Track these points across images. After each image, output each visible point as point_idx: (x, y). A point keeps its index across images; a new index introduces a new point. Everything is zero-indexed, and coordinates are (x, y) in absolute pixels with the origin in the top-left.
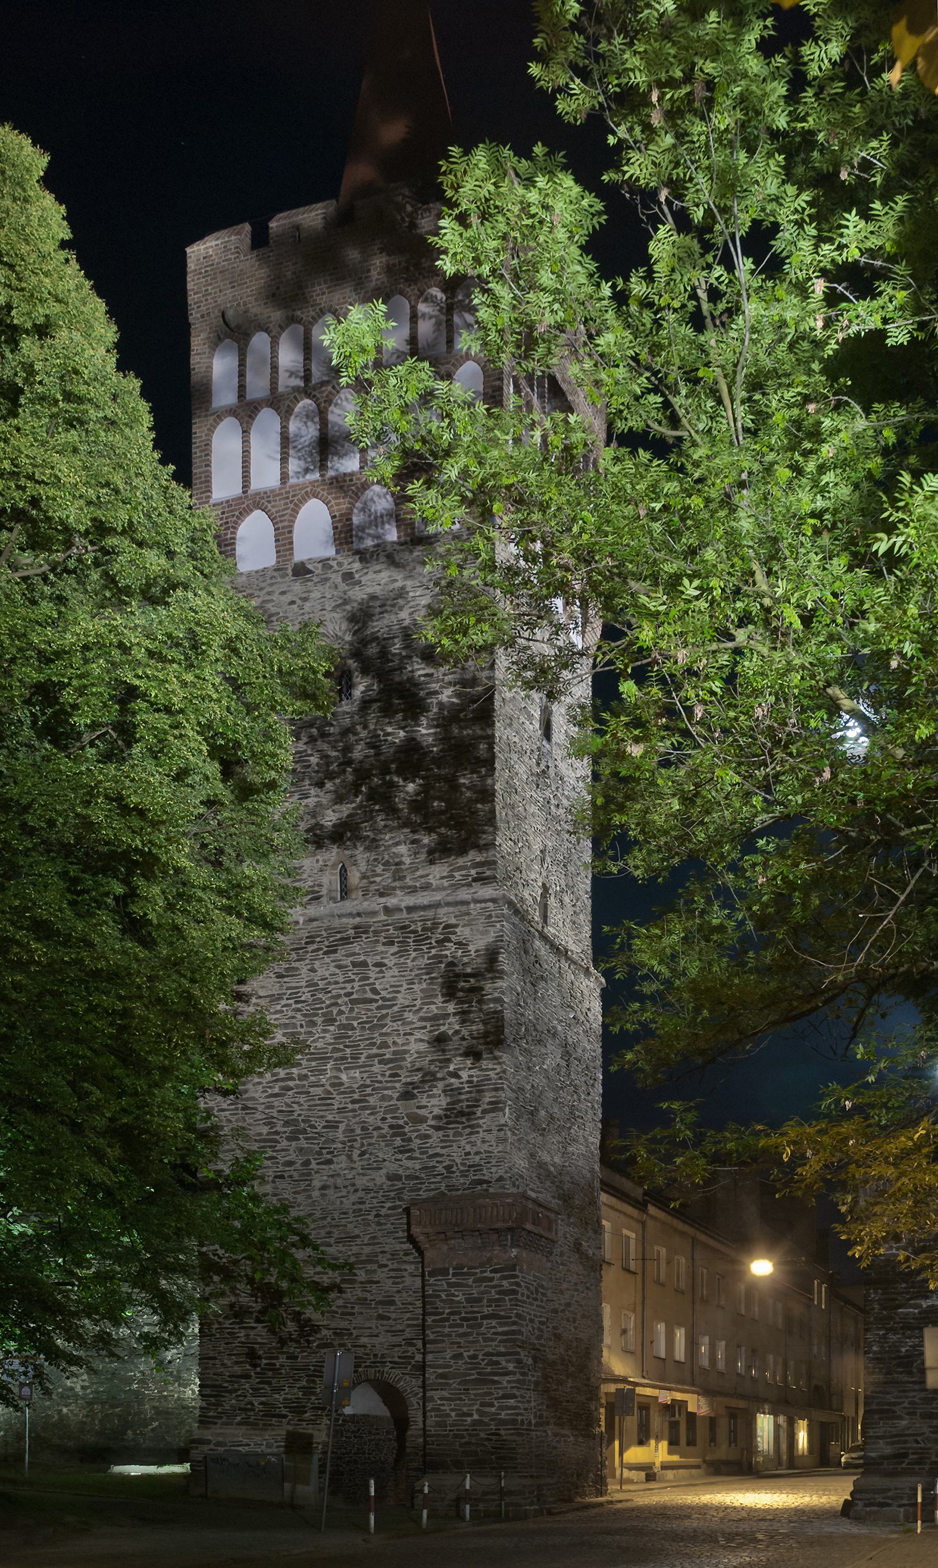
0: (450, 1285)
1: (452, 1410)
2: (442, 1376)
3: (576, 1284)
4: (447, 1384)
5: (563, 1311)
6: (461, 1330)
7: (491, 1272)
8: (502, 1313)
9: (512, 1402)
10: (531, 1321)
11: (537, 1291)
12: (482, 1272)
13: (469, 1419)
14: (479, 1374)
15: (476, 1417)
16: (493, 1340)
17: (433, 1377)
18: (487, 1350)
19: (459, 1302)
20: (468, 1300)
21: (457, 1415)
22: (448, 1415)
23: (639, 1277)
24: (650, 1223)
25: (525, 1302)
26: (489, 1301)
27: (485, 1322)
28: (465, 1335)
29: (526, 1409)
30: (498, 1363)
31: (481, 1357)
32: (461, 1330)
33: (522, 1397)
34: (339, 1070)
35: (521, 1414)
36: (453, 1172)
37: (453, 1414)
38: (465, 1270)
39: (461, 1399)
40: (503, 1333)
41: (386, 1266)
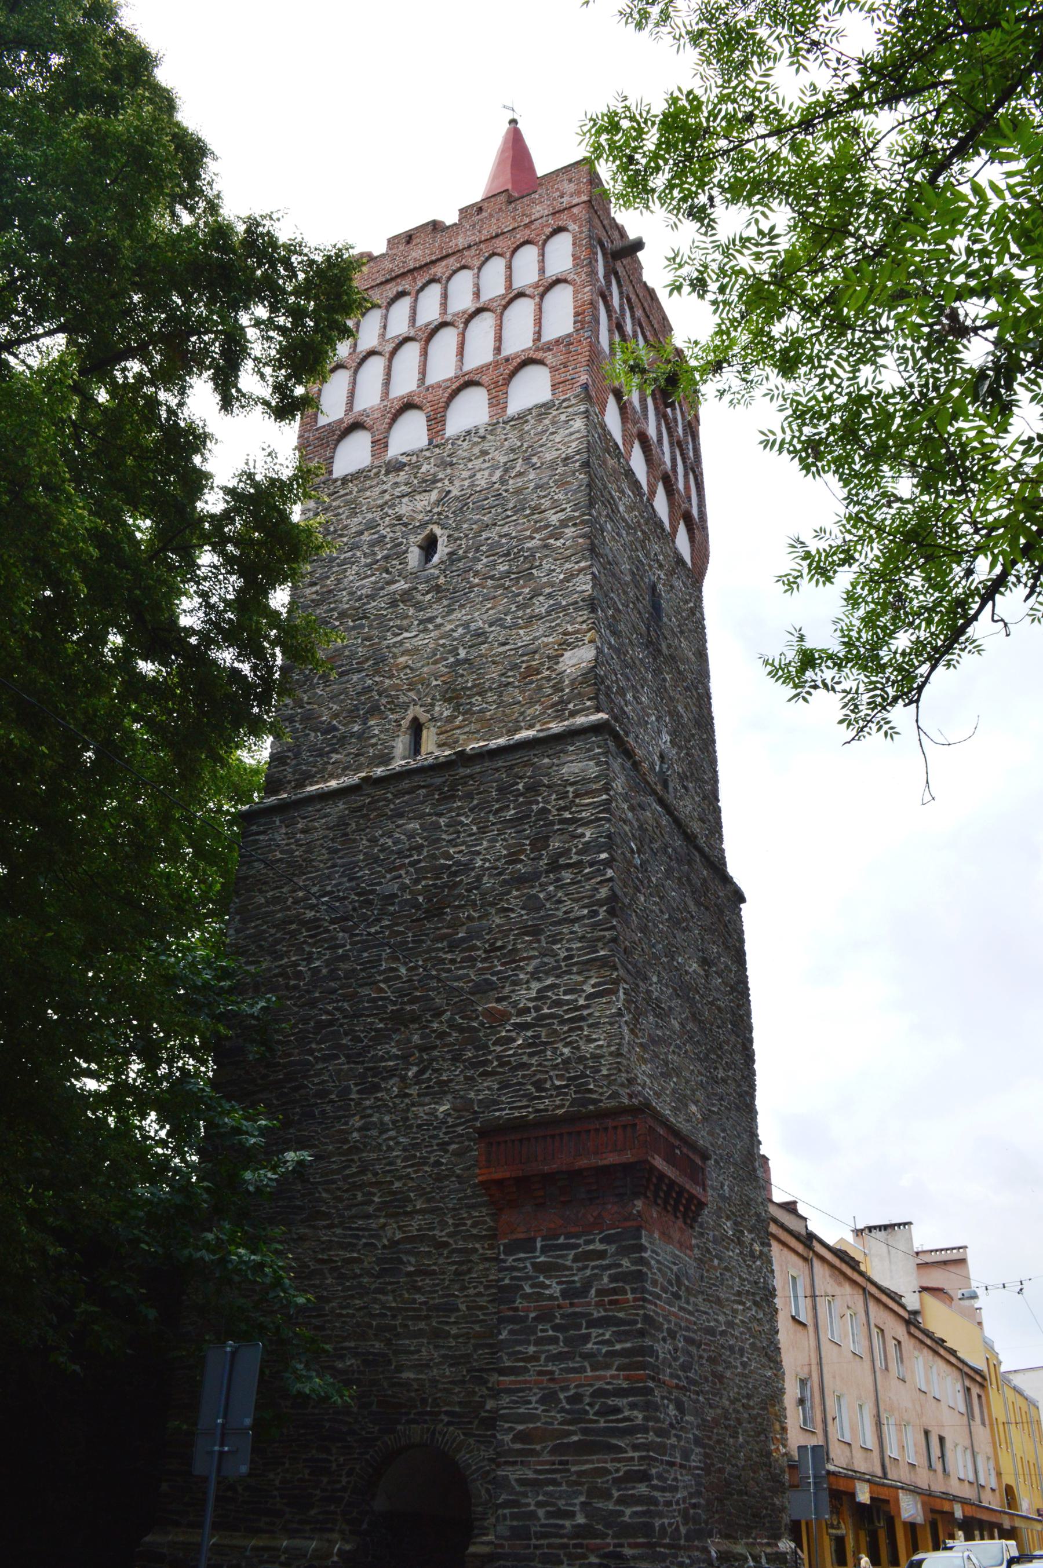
0: (539, 1268)
1: (539, 1504)
2: (520, 1437)
3: (739, 1294)
4: (533, 1453)
5: (723, 1333)
6: (554, 1349)
7: (601, 1241)
8: (621, 1315)
9: (642, 1489)
10: (672, 1334)
11: (679, 1283)
12: (588, 1242)
13: (568, 1523)
14: (585, 1431)
15: (581, 1520)
16: (607, 1367)
17: (507, 1438)
18: (599, 1384)
19: (551, 1297)
20: (564, 1294)
21: (549, 1515)
22: (533, 1515)
23: (811, 1329)
24: (817, 1264)
25: (659, 1297)
26: (599, 1292)
27: (594, 1332)
28: (560, 1357)
29: (668, 1504)
30: (617, 1410)
31: (587, 1400)
32: (554, 1349)
33: (660, 1477)
34: (397, 959)
35: (661, 1515)
36: (546, 1090)
37: (541, 1513)
38: (561, 1240)
39: (554, 1482)
40: (624, 1353)
41: (446, 1244)
